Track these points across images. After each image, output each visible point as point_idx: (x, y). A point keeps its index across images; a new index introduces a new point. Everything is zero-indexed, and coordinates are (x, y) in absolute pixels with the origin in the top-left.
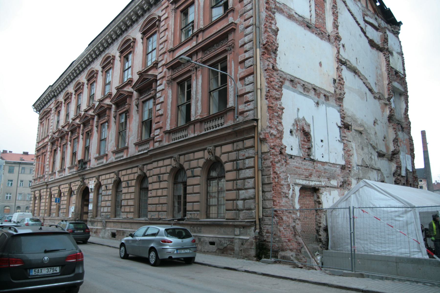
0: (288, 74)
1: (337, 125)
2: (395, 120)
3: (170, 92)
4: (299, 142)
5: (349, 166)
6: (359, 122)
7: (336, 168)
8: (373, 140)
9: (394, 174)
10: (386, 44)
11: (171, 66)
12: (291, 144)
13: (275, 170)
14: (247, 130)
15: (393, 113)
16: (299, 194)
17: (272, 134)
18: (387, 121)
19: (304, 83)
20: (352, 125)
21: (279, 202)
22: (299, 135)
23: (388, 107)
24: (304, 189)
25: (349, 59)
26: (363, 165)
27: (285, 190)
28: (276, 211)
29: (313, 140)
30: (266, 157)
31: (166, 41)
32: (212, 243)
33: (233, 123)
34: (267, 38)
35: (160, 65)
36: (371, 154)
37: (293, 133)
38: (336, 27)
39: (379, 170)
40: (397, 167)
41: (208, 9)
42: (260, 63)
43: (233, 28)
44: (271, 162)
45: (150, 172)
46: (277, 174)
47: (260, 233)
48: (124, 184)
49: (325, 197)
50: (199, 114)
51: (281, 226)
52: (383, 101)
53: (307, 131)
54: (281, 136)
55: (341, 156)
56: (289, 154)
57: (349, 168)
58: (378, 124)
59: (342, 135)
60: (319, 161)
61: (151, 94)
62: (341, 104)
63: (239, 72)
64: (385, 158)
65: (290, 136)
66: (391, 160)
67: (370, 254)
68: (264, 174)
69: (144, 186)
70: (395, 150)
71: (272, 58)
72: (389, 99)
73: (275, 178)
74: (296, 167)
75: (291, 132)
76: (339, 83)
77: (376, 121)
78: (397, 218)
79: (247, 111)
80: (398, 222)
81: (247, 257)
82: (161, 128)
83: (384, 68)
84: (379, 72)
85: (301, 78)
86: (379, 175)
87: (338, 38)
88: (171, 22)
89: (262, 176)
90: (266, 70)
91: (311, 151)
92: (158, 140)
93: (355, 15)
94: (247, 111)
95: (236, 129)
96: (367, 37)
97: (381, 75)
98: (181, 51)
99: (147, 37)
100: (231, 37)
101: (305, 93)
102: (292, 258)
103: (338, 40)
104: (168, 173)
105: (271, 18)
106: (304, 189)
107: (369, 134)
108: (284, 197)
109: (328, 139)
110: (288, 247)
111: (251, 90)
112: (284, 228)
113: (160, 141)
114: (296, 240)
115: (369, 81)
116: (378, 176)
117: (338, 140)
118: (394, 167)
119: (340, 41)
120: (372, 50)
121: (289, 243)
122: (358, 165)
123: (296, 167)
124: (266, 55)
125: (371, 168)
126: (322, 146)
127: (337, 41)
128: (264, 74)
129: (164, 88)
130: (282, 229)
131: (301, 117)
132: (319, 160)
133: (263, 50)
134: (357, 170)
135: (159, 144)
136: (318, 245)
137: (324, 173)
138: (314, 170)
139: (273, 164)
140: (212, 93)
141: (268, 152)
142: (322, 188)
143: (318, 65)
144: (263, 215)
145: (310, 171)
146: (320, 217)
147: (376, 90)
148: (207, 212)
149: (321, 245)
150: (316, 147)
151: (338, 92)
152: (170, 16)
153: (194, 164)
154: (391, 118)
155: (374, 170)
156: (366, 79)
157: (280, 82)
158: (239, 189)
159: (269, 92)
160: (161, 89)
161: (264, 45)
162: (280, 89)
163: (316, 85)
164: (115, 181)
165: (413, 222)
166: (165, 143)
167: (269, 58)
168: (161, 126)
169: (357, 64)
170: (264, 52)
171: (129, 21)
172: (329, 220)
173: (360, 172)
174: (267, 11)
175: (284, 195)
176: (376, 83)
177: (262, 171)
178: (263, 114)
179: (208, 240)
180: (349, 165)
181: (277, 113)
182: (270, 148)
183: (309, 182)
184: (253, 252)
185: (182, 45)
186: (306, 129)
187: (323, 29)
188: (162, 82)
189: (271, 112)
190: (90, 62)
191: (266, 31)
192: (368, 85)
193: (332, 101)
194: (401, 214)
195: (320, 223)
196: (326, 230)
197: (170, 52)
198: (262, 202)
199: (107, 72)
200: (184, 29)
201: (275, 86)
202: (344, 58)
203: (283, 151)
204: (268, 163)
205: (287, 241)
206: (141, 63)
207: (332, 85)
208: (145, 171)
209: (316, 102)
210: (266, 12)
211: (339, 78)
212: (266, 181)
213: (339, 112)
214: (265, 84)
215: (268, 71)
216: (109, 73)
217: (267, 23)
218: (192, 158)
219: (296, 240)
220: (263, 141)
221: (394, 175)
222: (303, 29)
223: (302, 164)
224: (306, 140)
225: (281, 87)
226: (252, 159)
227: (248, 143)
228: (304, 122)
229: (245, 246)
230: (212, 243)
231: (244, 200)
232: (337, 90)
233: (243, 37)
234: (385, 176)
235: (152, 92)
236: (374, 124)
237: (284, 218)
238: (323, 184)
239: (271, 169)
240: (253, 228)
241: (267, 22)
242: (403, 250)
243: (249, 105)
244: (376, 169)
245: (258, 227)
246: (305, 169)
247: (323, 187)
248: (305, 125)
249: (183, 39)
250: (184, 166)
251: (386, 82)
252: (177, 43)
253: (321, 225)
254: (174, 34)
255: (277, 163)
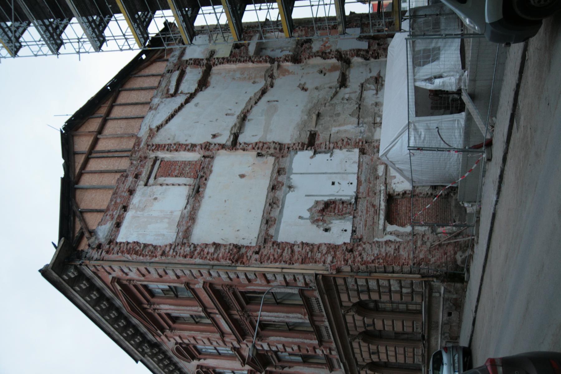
0: (260, 227)
1: (312, 157)
2: (297, 50)
3: (272, 339)
4: (337, 219)
5: (361, 143)
6: (306, 117)
7: (364, 163)
8: (325, 94)
9: (367, 59)
10: (201, 62)
11: (242, 336)
12: (340, 232)
13: (371, 261)
14: (327, 285)
15: (290, 58)
16: (395, 226)
17: (332, 262)
18: (299, 65)
19: (268, 205)
20: (309, 129)
21: (405, 260)
22: (329, 218)
23: (281, 64)
24: (390, 218)
25: (230, 128)
26: (357, 115)
27: (391, 250)
28: (414, 264)
29: (333, 198)
30: (356, 268)
31: (209, 339)
32: (450, 314)
33: (317, 291)
34: (226, 260)
35: (237, 346)
36: (343, 99)
37: (327, 227)
38: (192, 147)
39: (362, 85)
40: (358, 55)
41: (179, 302)
42: (253, 267)
43: (209, 287)
44: (362, 265)
45: (357, 320)
46: (374, 259)
47: (437, 277)
48: (375, 358)
49: (398, 185)
50: (303, 317)
51: (430, 260)
52: (275, 71)
53: (323, 206)
54: (333, 248)
55: (349, 153)
56: (350, 235)
57: (362, 142)
58: (305, 83)
59: (323, 149)
60: (357, 190)
61: (272, 356)
62: (286, 147)
63: (260, 283)
64: (347, 73)
65: (331, 232)
66: (348, 62)
67: (461, 160)
68: (374, 270)
69: (372, 305)
70: (336, 57)
71: (246, 252)
72: (272, 60)
73: (378, 262)
74: (366, 226)
75: (326, 230)
76: (262, 149)
77: (301, 86)
78: (423, 136)
79: (305, 280)
80: (426, 136)
81: (464, 290)
82: (314, 349)
83: (233, 66)
84: (238, 75)
85: (263, 208)
86: (368, 86)
87: (206, 146)
88: (186, 334)
89: (376, 272)
90: (261, 263)
91: (346, 202)
92: (328, 351)
93: (171, 111)
94: (305, 280)
95: (324, 291)
96: (197, 91)
97: (243, 71)
98: (223, 324)
99: (198, 354)
100: (219, 287)
101: (281, 206)
102: (463, 257)
103: (209, 147)
104: (369, 345)
105: (202, 253)
106: (390, 218)
107: (318, 101)
108: (399, 252)
109: (331, 173)
110: (453, 256)
111: (283, 276)
112: (433, 257)
113: (330, 349)
114: (445, 246)
115: (253, 95)
116: (370, 89)
117: (331, 156)
118: (356, 60)
119: (210, 144)
120: (212, 85)
121: (448, 254)
122: (358, 124)
123: (366, 226)
124: (244, 260)
125: (360, 100)
126: (339, 183)
127: (210, 148)
128: (265, 264)
129: (266, 344)
130: (433, 260)
131: (307, 215)
132: (355, 190)
133: (239, 263)
134: (364, 125)
135: (333, 350)
136: (452, 197)
137: (370, 183)
138: (368, 198)
139: (365, 263)
140: (278, 301)
141: (351, 267)
142: (388, 190)
143: (243, 180)
144: (418, 274)
145: (369, 205)
146: (421, 193)
147: (261, 84)
148: (414, 313)
149: (452, 194)
150: (341, 193)
151: (272, 151)
152: (178, 334)
153: (359, 323)
154: (296, 60)
155: (363, 96)
156: (250, 99)
157: (273, 246)
158: (390, 291)
159: (285, 262)
160: (267, 346)
161: (233, 262)
162: (281, 246)
163: (268, 185)
164: (365, 341)
165: (427, 124)
166: (334, 346)
167: (247, 256)
168: (311, 348)
169: (233, 115)
170: (241, 263)
171: (165, 362)
172: (424, 184)
173: (366, 120)
174: (194, 257)
175: (397, 252)
176: (252, 81)
177: (371, 272)
178: (310, 269)
179: (446, 317)
180: (359, 143)
181: (308, 253)
182: (347, 264)
183: (382, 209)
184: (458, 285)
185: (215, 323)
186: (321, 206)
187: (198, 167)
188: (258, 345)
189: (307, 260)
190: (170, 363)
191: (217, 260)
192: (258, 97)
193: (285, 163)
194: (418, 134)
195: (427, 194)
196: (434, 187)
197: (224, 337)
198: (405, 274)
199: (200, 352)
200: (195, 319)
201: (279, 253)
202: (230, 137)
203: (349, 248)
204: (363, 267)
205: (446, 256)
206: (230, 362)
207: (264, 159)
208: (351, 304)
209: (288, 189)
210: (195, 258)
211: (256, 148)
212: (383, 270)
213: (296, 151)
214: (277, 265)
215: (263, 261)
216: (202, 349)
217: (208, 258)
218: (353, 325)
219: (445, 246)
220: (339, 271)
221: (368, 60)
222: (203, 200)
223: (361, 216)
224: (333, 206)
225: (278, 245)
226: (358, 280)
227: (340, 281)
228: (314, 210)
229: (452, 290)
230: (450, 314)
231: (401, 287)
232: (270, 152)
233: (221, 277)
234: (369, 75)
235: (269, 354)
236: (306, 90)
237: (421, 256)
238: (383, 188)
239: (369, 265)
240: (432, 283)
241: (206, 257)
242: (457, 134)
243: (298, 278)
244: (362, 92)
245: (431, 279)
246: (367, 214)
247: (386, 187)
248: (317, 208)
249: (209, 321)
250: (361, 331)
251: (250, 65)
252: (214, 329)
253: (429, 193)
254: (202, 331)
255: (363, 258)
